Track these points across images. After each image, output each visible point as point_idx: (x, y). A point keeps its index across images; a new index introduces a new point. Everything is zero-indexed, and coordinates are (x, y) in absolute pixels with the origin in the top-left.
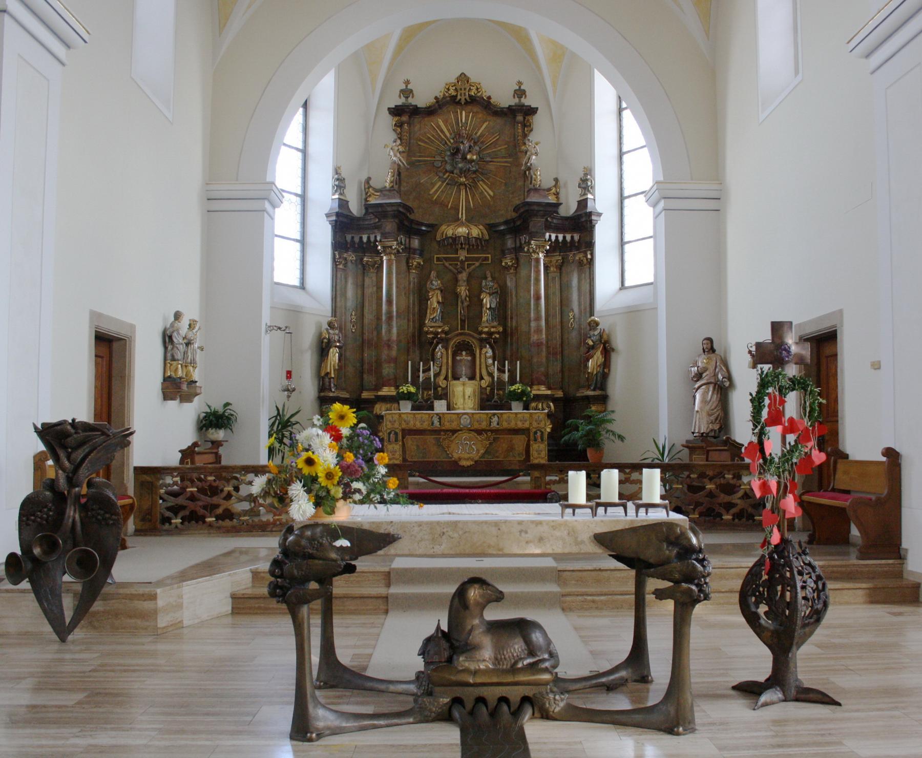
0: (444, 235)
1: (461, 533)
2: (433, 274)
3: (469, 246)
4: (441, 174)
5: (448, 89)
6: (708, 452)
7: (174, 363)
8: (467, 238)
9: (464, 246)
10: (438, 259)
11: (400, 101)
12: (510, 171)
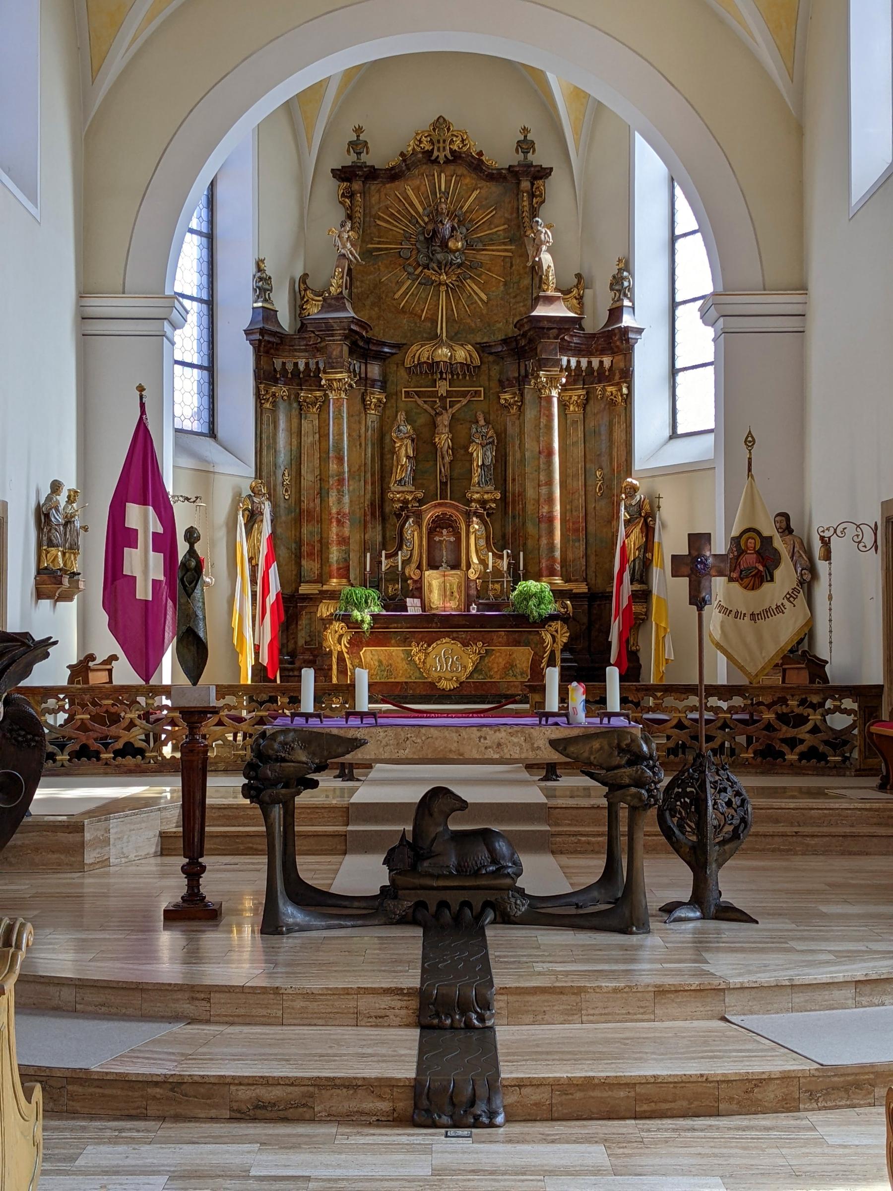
0: (416, 360)
1: (423, 738)
2: (401, 416)
3: (453, 376)
4: (411, 270)
5: (420, 142)
6: (784, 670)
7: (53, 550)
8: (451, 366)
9: (444, 376)
10: (407, 394)
11: (349, 160)
12: (511, 263)
